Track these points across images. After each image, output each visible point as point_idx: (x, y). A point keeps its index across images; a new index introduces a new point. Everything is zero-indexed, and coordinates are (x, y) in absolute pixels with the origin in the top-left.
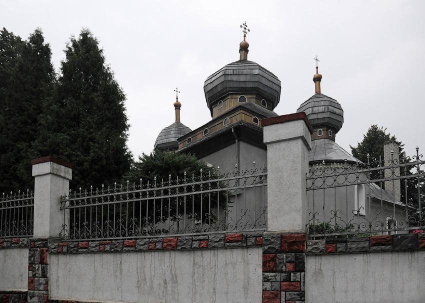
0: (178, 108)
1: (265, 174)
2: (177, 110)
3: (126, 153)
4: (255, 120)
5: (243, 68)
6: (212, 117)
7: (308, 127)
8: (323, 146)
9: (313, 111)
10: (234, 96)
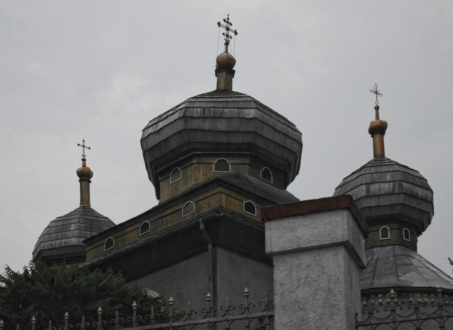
0: (84, 180)
1: (270, 313)
2: (84, 183)
3: (30, 273)
4: (249, 207)
5: (224, 105)
6: (158, 198)
7: (359, 225)
8: (392, 259)
9: (368, 190)
10: (206, 160)
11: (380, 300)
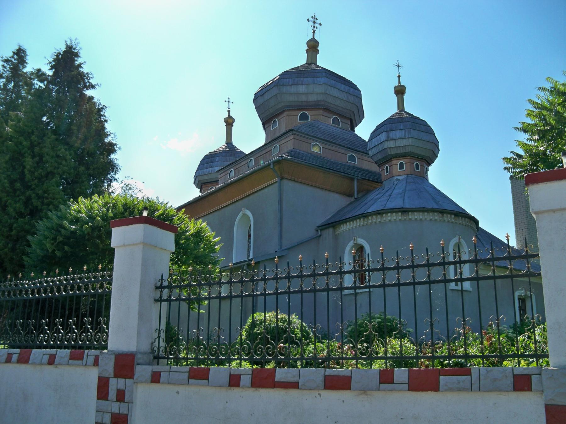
9: (388, 137)
11: (389, 218)
